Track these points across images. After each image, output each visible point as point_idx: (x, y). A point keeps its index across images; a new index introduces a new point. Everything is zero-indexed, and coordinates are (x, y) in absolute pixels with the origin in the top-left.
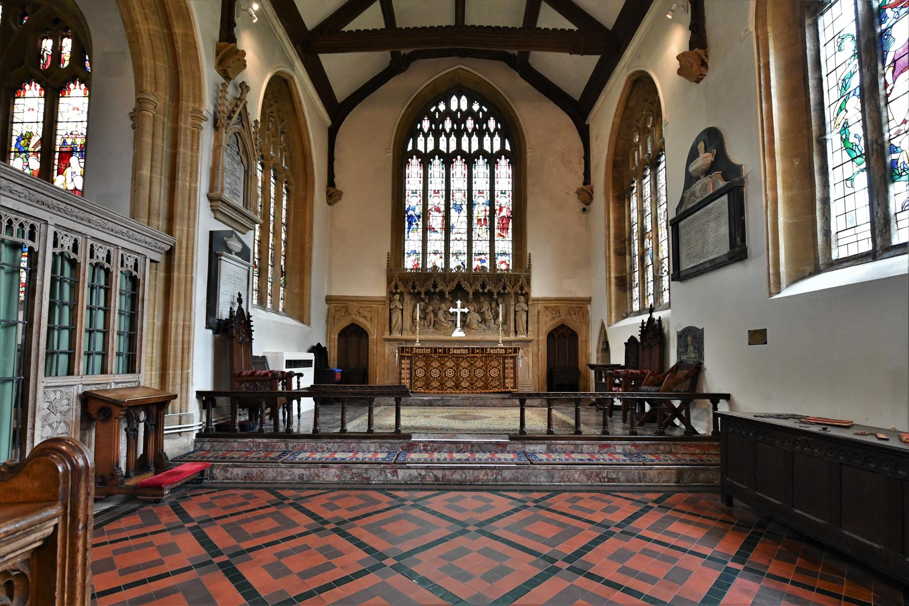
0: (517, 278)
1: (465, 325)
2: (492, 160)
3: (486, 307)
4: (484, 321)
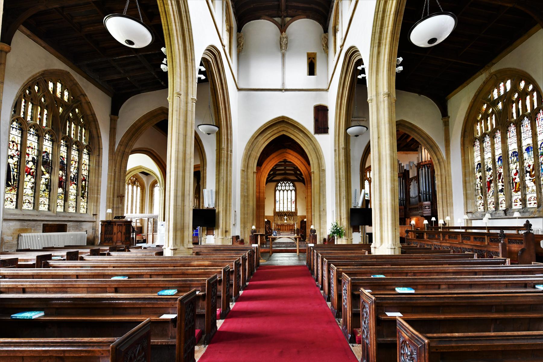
0: (294, 212)
2: (291, 191)
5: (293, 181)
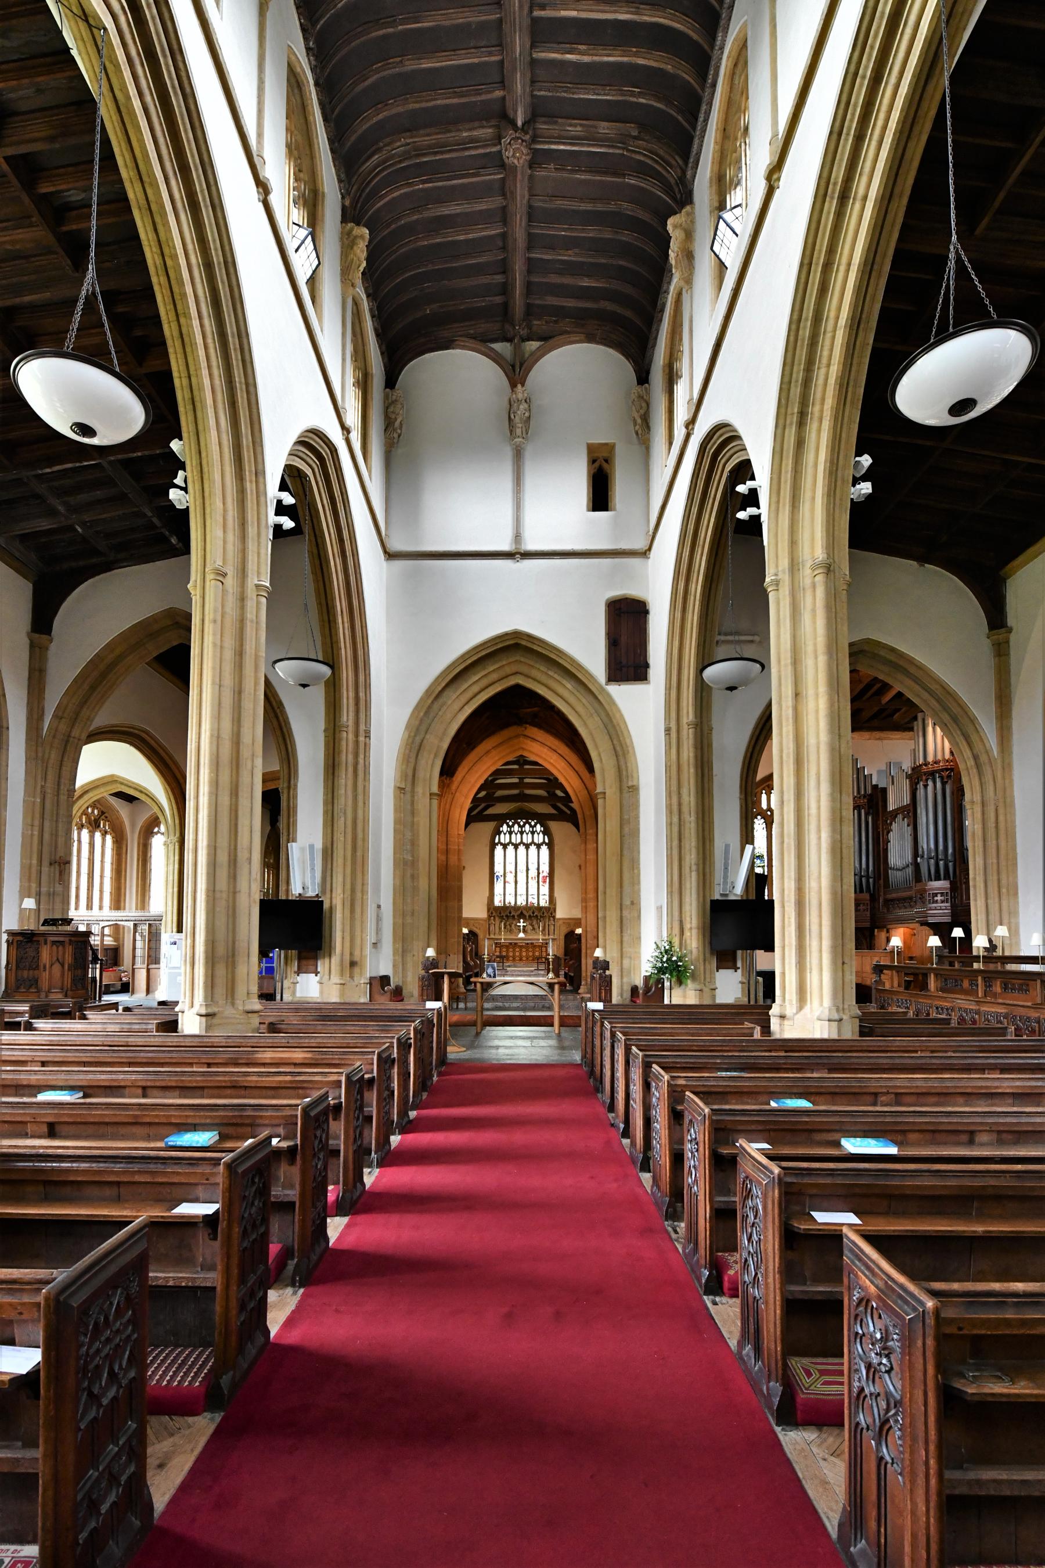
1: (524, 931)
2: (538, 846)
3: (535, 923)
4: (534, 929)
5: (542, 819)
